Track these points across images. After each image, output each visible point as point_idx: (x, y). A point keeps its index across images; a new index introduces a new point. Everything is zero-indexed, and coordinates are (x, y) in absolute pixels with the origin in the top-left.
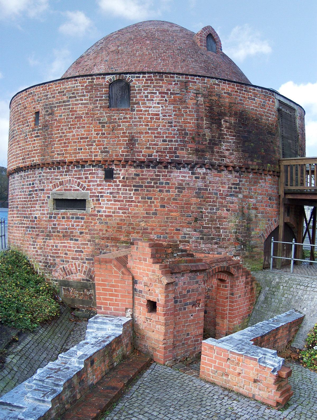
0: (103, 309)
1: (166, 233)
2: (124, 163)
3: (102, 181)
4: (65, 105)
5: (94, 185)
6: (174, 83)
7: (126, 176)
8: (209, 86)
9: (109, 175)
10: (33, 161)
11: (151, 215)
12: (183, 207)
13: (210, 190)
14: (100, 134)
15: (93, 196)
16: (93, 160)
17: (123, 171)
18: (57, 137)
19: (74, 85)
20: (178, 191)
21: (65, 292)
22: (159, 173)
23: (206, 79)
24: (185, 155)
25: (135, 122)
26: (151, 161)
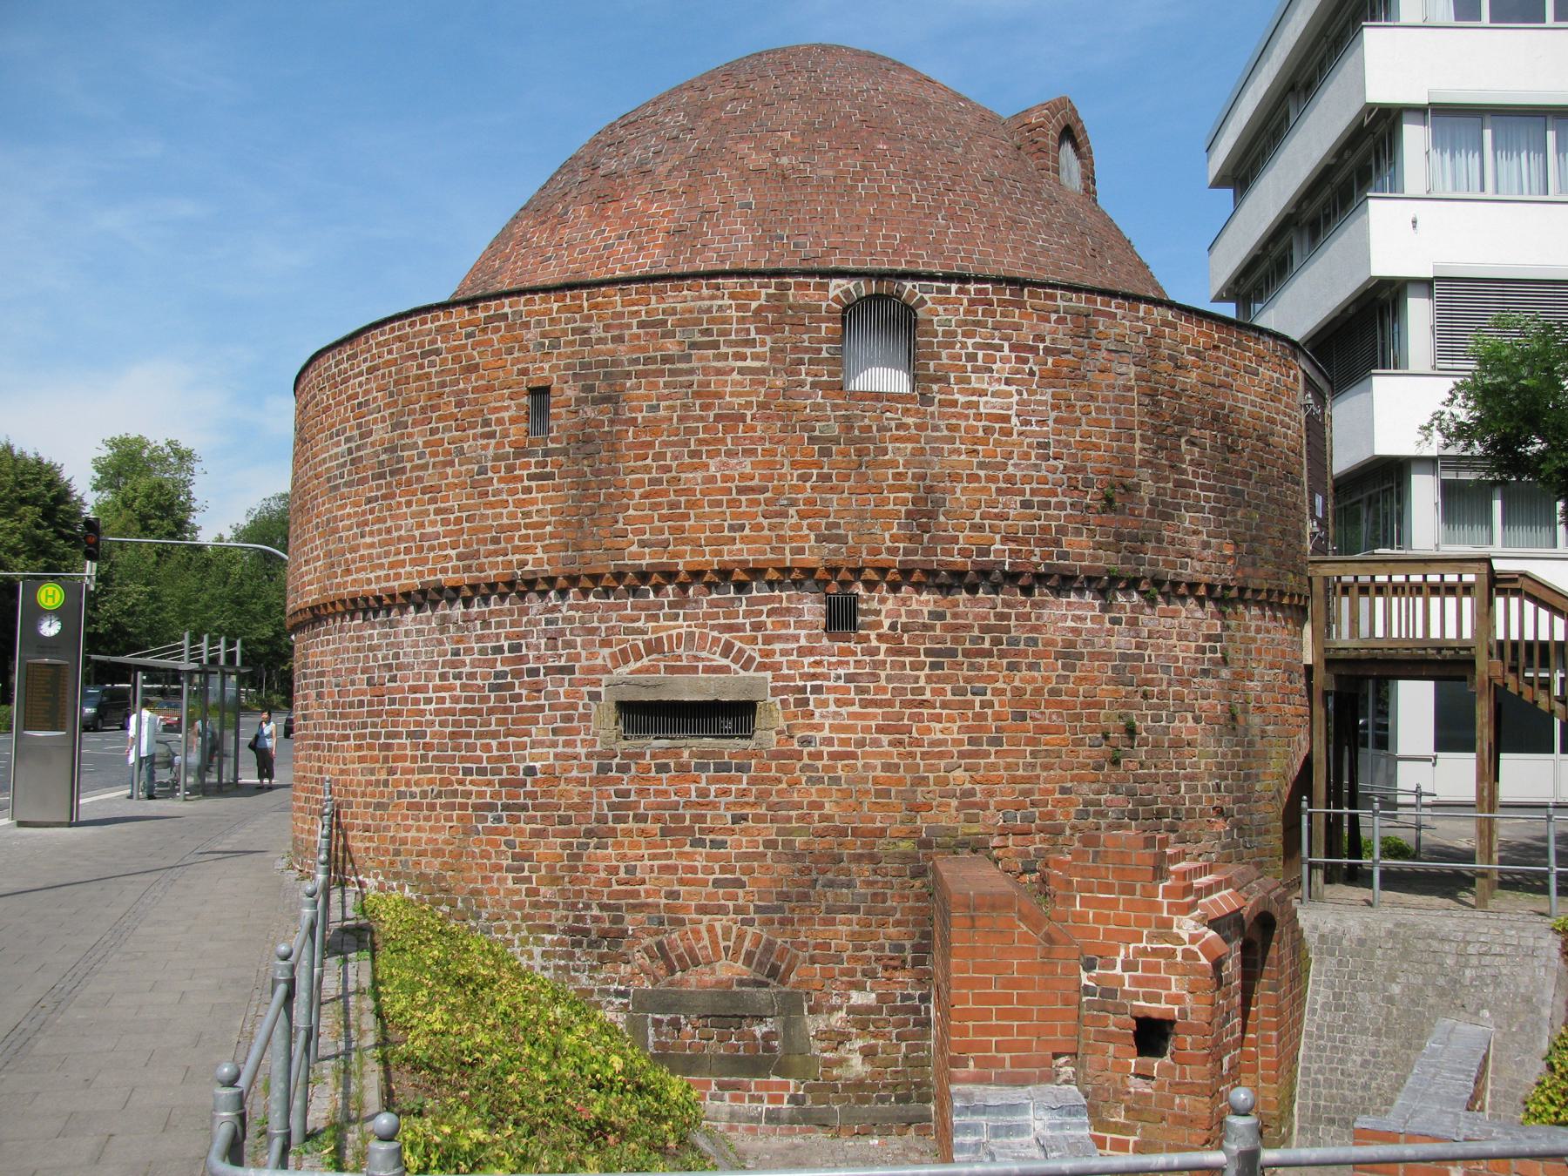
0: (971, 1063)
1: (1033, 804)
2: (898, 578)
3: (818, 638)
4: (672, 373)
5: (784, 653)
6: (1054, 317)
7: (900, 621)
8: (1149, 328)
9: (842, 618)
10: (523, 563)
11: (985, 747)
12: (1078, 717)
13: (1150, 660)
14: (814, 478)
15: (784, 690)
16: (788, 564)
17: (890, 605)
18: (640, 483)
19: (707, 303)
20: (1064, 667)
21: (658, 1033)
22: (1009, 606)
23: (1142, 307)
24: (1086, 552)
25: (937, 439)
26: (984, 573)
